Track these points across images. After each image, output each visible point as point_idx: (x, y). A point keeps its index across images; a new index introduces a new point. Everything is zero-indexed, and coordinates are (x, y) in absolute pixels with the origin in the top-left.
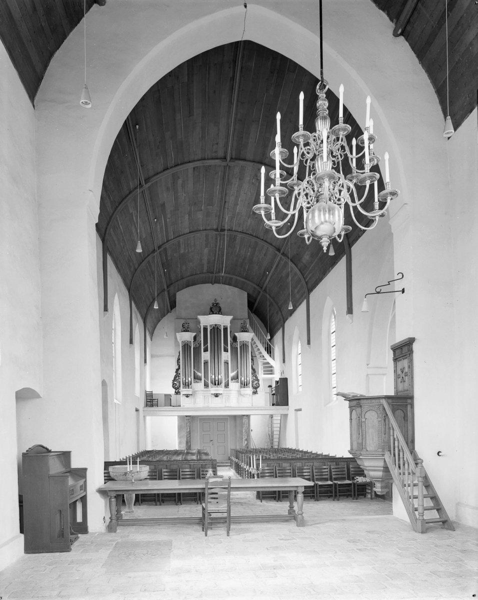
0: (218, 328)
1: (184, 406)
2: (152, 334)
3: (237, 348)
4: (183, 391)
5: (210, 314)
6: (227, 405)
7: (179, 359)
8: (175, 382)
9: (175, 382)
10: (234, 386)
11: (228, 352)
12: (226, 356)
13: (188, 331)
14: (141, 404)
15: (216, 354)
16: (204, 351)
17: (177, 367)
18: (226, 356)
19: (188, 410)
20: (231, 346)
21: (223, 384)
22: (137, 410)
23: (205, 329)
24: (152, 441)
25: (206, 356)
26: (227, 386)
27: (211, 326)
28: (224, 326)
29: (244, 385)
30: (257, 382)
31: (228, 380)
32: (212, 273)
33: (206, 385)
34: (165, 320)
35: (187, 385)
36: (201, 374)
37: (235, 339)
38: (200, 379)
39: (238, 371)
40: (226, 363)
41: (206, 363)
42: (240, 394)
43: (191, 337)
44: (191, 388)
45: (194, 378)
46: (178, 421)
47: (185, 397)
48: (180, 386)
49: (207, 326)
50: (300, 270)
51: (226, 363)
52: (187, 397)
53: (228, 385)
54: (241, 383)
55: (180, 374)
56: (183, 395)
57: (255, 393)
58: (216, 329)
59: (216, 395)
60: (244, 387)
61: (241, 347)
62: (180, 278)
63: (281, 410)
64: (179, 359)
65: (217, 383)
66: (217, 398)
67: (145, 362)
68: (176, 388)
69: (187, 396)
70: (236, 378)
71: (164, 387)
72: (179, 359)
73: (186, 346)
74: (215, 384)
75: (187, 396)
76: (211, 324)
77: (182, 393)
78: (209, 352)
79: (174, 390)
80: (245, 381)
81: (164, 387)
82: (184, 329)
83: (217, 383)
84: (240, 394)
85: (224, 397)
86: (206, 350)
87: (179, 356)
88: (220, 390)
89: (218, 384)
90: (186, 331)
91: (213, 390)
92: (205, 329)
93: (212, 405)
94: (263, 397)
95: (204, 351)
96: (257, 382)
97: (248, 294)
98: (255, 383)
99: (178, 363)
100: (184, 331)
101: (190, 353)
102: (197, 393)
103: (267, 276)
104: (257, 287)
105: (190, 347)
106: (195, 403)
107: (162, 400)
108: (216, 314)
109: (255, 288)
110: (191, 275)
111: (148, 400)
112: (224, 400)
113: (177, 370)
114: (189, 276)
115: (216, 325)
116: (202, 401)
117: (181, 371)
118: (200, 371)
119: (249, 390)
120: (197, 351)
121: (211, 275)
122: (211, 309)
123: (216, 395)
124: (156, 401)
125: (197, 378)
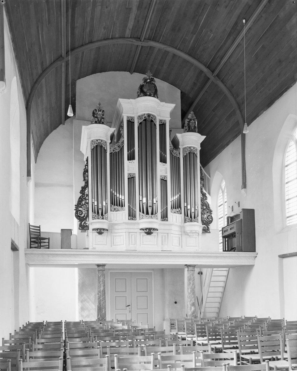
0: (152, 121)
1: (94, 248)
2: (37, 151)
3: (179, 158)
4: (93, 223)
5: (138, 96)
6: (166, 248)
7: (86, 171)
8: (80, 209)
9: (80, 209)
10: (175, 218)
11: (165, 162)
12: (163, 170)
13: (103, 123)
14: (22, 242)
15: (148, 167)
16: (128, 160)
17: (83, 184)
18: (163, 170)
19: (102, 254)
20: (171, 153)
21: (159, 215)
22: (14, 248)
23: (130, 123)
24: (37, 307)
25: (131, 167)
26: (165, 217)
27: (139, 117)
28: (161, 121)
29: (190, 217)
30: (208, 214)
31: (167, 208)
32: (138, 39)
33: (132, 215)
34: (54, 135)
35: (100, 213)
36: (124, 197)
37: (175, 144)
38: (122, 205)
39: (180, 196)
40: (164, 181)
41: (131, 179)
42: (184, 233)
43: (106, 135)
44: (107, 219)
45: (112, 203)
46: (80, 275)
47: (95, 233)
48: (88, 216)
49: (133, 118)
50: (228, 88)
51: (164, 181)
52: (100, 233)
53: (167, 217)
54: (186, 215)
55: (88, 195)
56: (93, 230)
57: (206, 230)
58: (148, 122)
59: (149, 231)
60: (191, 221)
61: (185, 158)
62: (87, 42)
63: (239, 258)
64: (87, 171)
65: (148, 211)
66: (149, 236)
67: (29, 174)
68: (82, 219)
69: (100, 231)
70: (177, 206)
71: (58, 217)
72: (86, 171)
73: (98, 149)
74: (147, 213)
75: (100, 231)
76: (140, 114)
77: (91, 227)
78: (136, 161)
79: (76, 222)
80: (193, 211)
81: (58, 217)
82: (96, 119)
83: (150, 210)
84: (184, 232)
85: (160, 235)
86: (131, 157)
87: (87, 165)
88: (154, 222)
89: (152, 214)
90: (99, 123)
91: (145, 222)
92: (130, 123)
93: (140, 247)
94: (215, 241)
95: (128, 160)
96: (208, 214)
97: (181, 92)
98: (205, 216)
99: (84, 177)
100: (96, 122)
101: (104, 162)
102: (116, 227)
103: (243, 26)
104: (205, 70)
105: (105, 151)
106: (112, 244)
107: (57, 240)
108: (150, 95)
109: (201, 72)
110: (105, 39)
111: (32, 240)
112: (160, 239)
113: (84, 189)
114: (101, 40)
115: (149, 115)
116: (123, 240)
117: (89, 191)
118: (121, 192)
119: (198, 226)
120: (117, 158)
121: (136, 43)
122: (141, 87)
123: (149, 231)
124: (47, 241)
125: (116, 203)
